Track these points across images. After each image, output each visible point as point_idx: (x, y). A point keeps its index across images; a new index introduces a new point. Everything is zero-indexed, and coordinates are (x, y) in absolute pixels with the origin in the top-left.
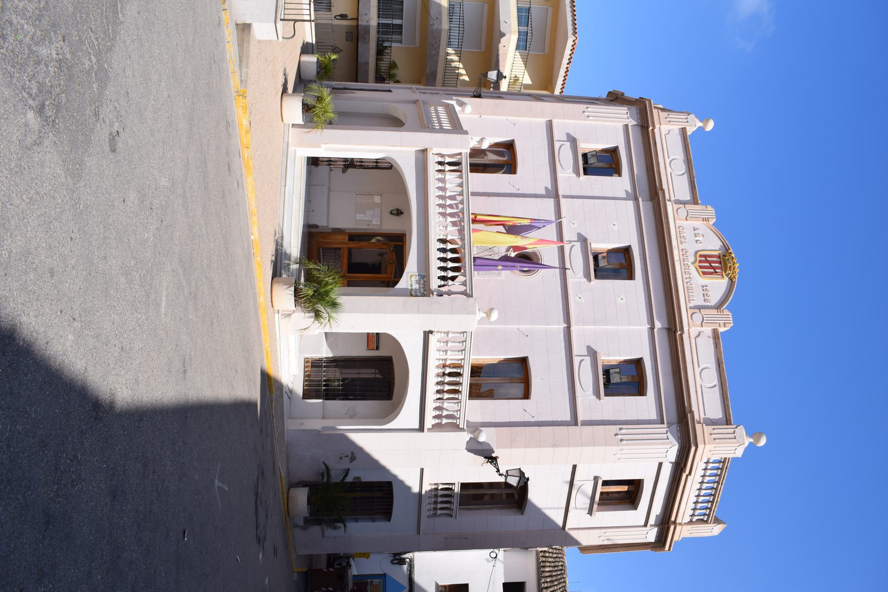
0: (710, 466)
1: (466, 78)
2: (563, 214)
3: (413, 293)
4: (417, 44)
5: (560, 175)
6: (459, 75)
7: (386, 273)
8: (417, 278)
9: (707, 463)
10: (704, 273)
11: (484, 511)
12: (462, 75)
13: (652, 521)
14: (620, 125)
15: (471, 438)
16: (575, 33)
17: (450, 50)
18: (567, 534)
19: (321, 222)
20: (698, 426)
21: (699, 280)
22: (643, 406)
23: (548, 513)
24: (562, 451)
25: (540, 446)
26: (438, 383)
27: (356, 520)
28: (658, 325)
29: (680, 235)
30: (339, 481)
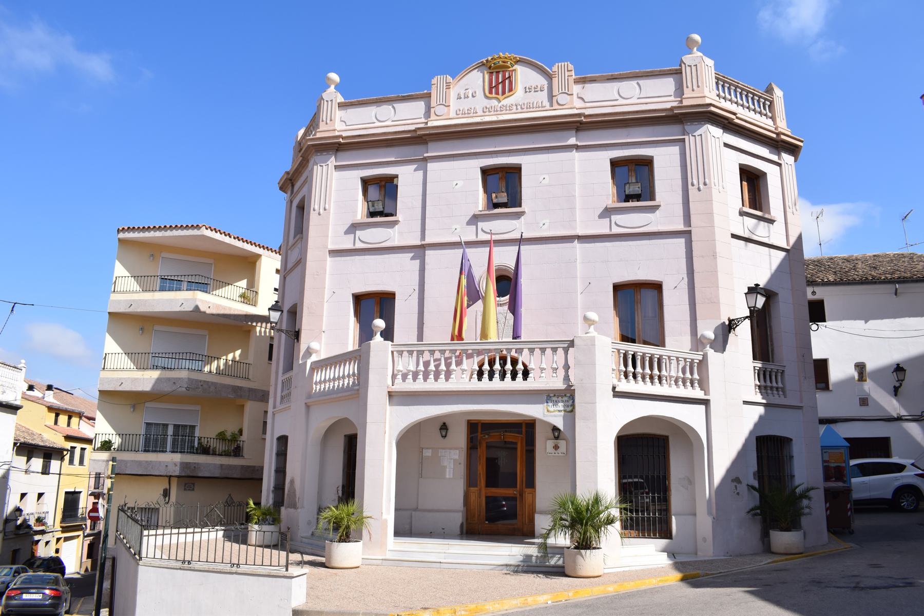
0: (722, 94)
1: (238, 353)
2: (457, 239)
3: (570, 409)
4: (198, 408)
5: (396, 243)
6: (234, 360)
7: (516, 443)
8: (550, 404)
9: (718, 95)
10: (511, 90)
11: (774, 336)
12: (234, 357)
13: (774, 158)
14: (336, 175)
15: (711, 347)
16: (198, 227)
17: (207, 369)
18: (793, 247)
19: (458, 519)
20: (685, 103)
21: (518, 96)
22: (665, 161)
23: (775, 266)
24: (719, 248)
25: (716, 272)
26: (652, 383)
27: (793, 477)
28: (572, 141)
30: (757, 495)
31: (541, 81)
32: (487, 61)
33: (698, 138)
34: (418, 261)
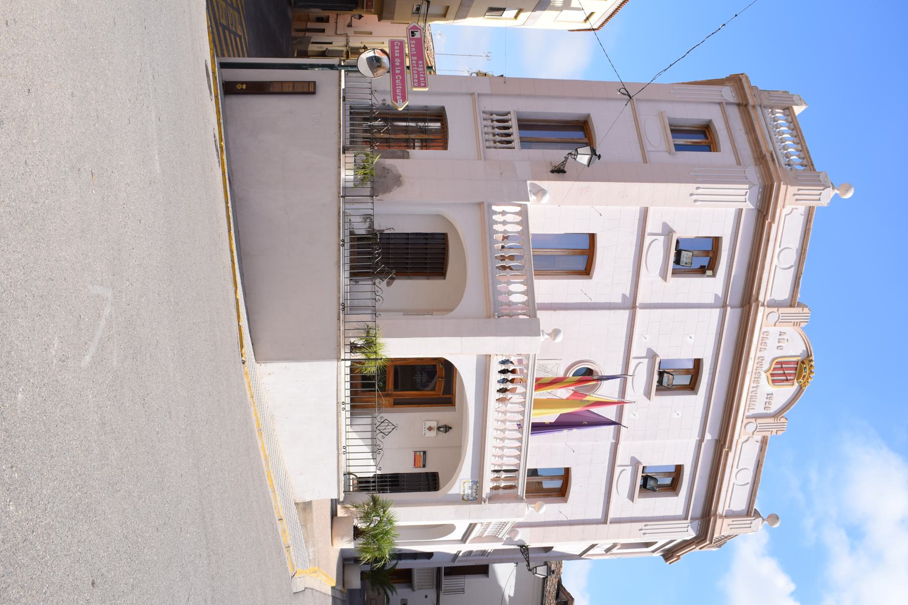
3: (465, 498)
14: (731, 211)
21: (766, 386)
28: (708, 436)
29: (763, 342)
31: (775, 407)
32: (811, 361)
33: (743, 198)
34: (620, 301)
